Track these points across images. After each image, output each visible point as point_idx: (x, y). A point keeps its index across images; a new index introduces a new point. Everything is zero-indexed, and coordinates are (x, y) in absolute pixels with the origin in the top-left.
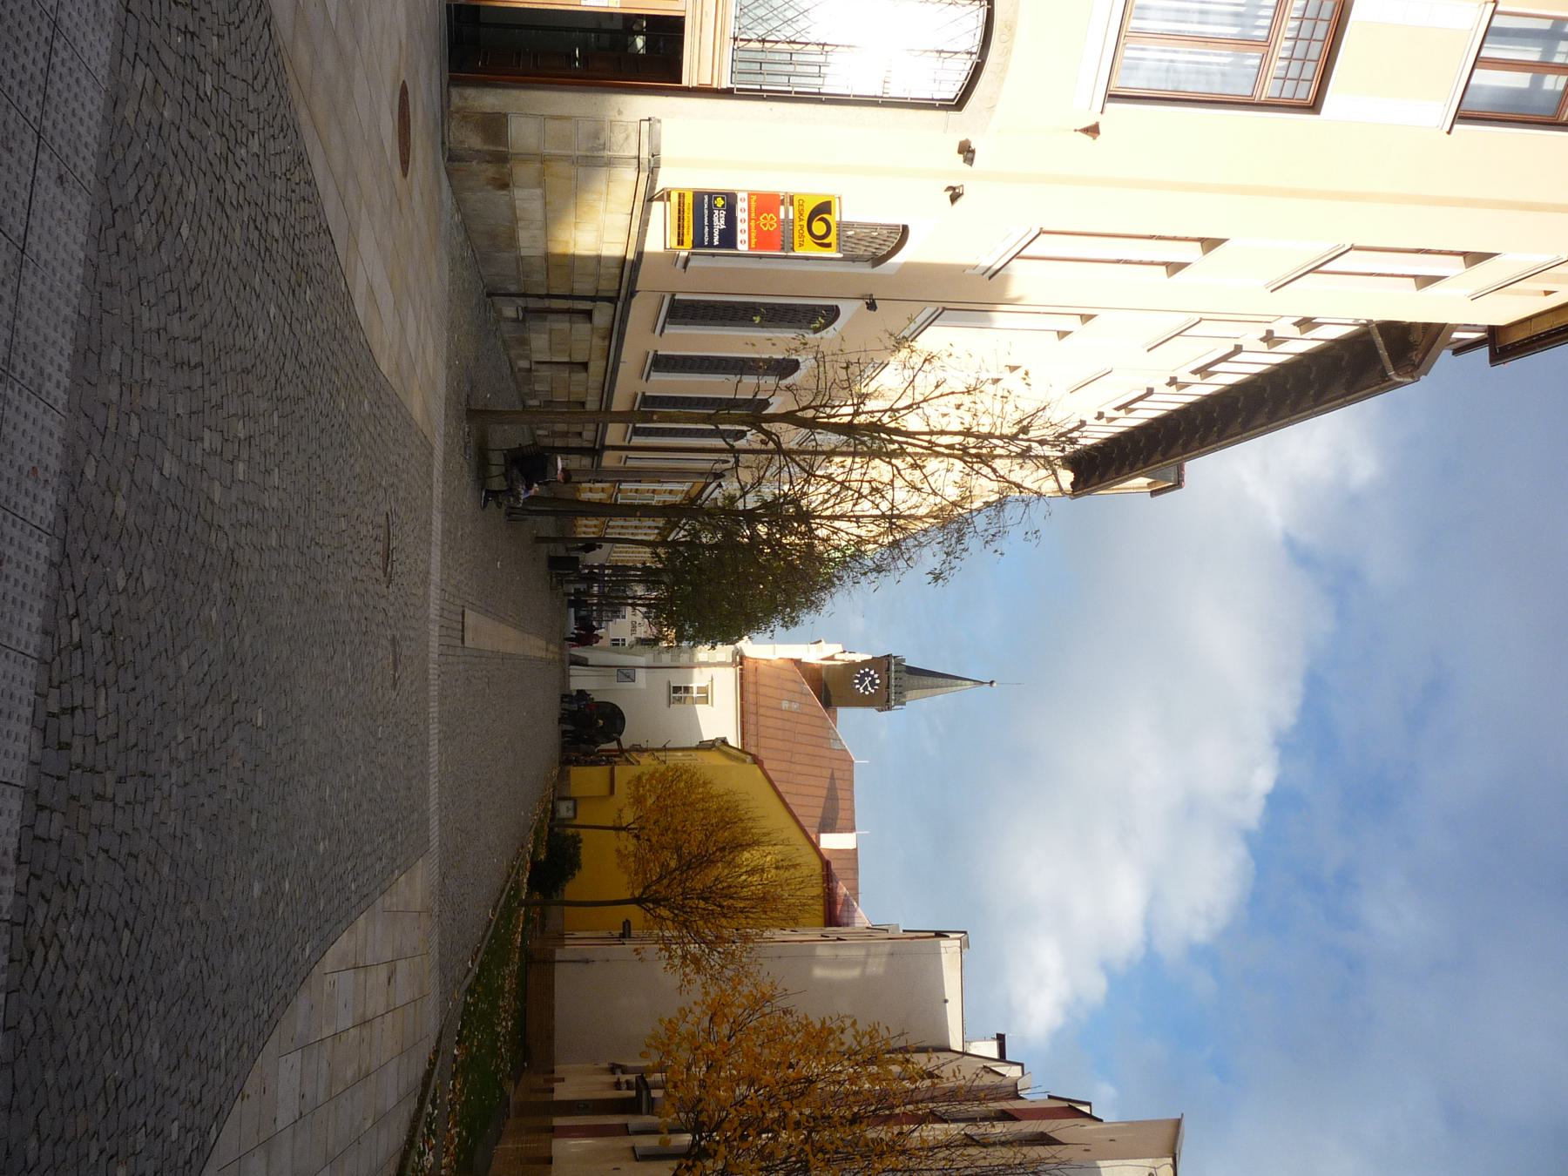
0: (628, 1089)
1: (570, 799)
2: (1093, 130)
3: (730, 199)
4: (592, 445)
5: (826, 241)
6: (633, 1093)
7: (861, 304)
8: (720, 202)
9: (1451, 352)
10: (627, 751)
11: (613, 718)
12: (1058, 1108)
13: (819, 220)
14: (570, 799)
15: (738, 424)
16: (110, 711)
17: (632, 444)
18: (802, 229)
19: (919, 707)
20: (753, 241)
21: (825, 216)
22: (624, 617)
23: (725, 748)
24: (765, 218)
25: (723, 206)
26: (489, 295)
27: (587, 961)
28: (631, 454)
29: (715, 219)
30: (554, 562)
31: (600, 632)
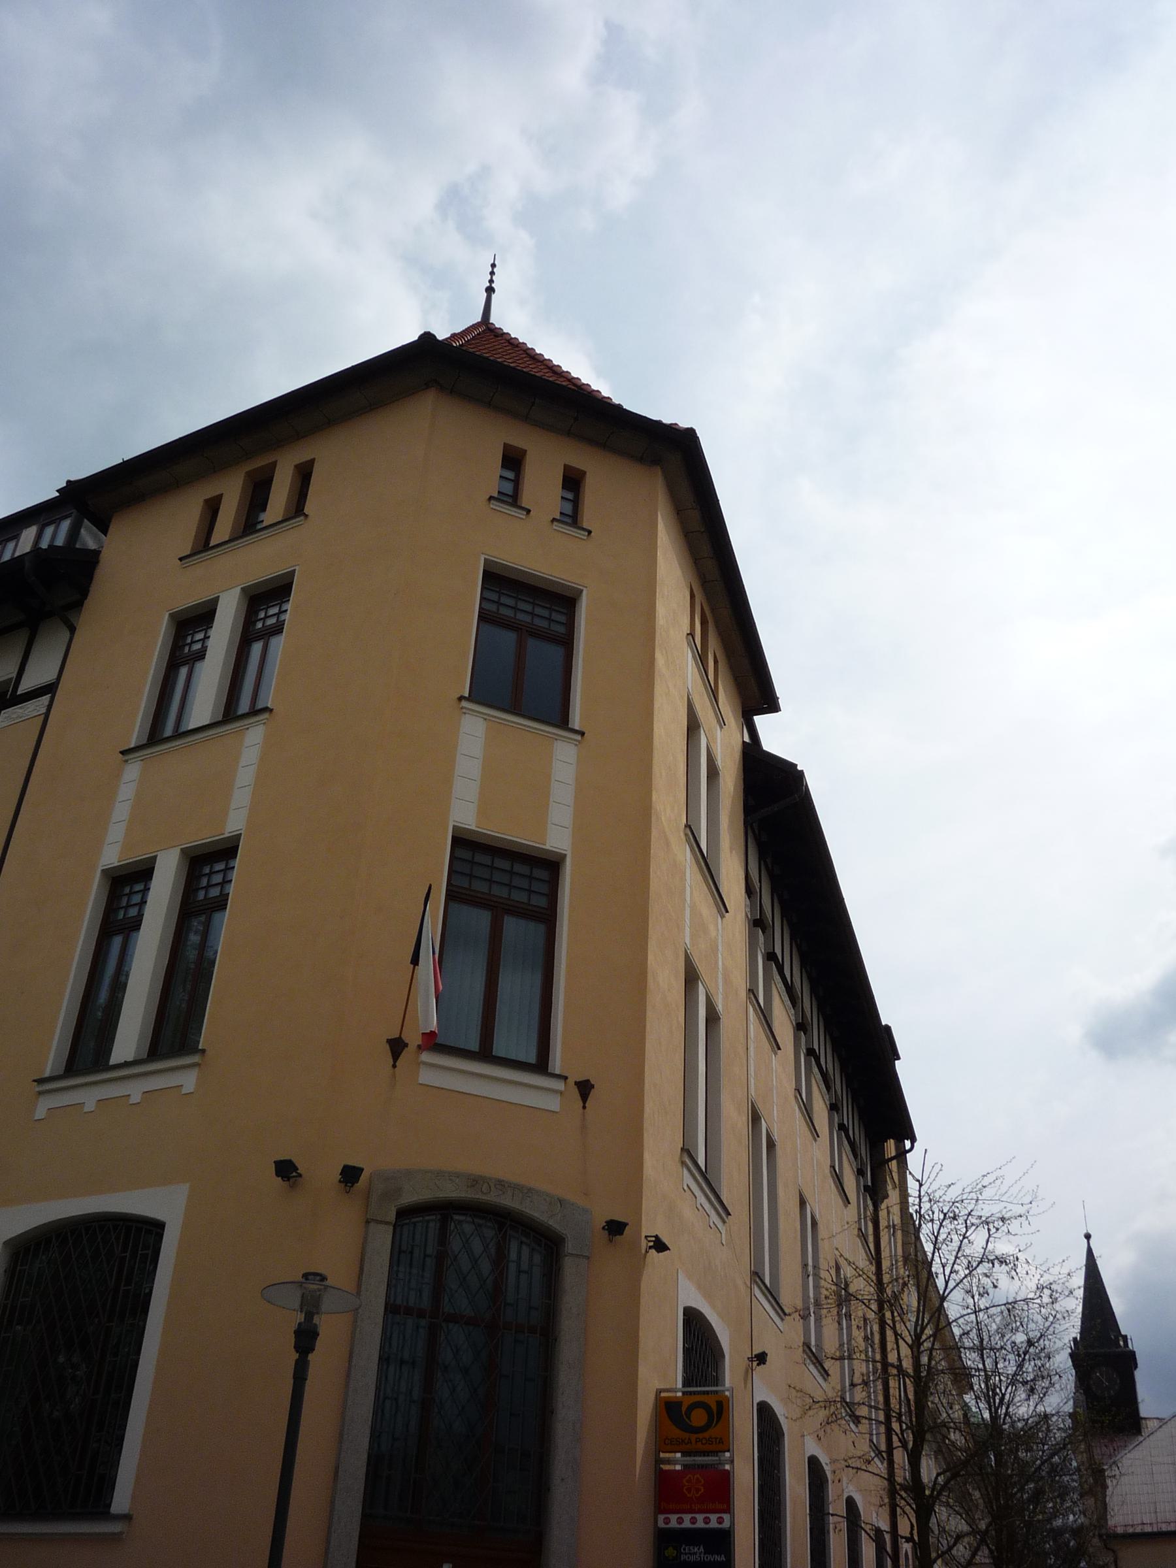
2: (585, 1088)
3: (665, 1538)
7: (760, 1370)
8: (670, 1552)
9: (779, 1051)
13: (689, 1418)
15: (730, 1359)
16: (1064, 1296)
19: (808, 1195)
21: (684, 1409)
24: (689, 1490)
31: (605, 1224)
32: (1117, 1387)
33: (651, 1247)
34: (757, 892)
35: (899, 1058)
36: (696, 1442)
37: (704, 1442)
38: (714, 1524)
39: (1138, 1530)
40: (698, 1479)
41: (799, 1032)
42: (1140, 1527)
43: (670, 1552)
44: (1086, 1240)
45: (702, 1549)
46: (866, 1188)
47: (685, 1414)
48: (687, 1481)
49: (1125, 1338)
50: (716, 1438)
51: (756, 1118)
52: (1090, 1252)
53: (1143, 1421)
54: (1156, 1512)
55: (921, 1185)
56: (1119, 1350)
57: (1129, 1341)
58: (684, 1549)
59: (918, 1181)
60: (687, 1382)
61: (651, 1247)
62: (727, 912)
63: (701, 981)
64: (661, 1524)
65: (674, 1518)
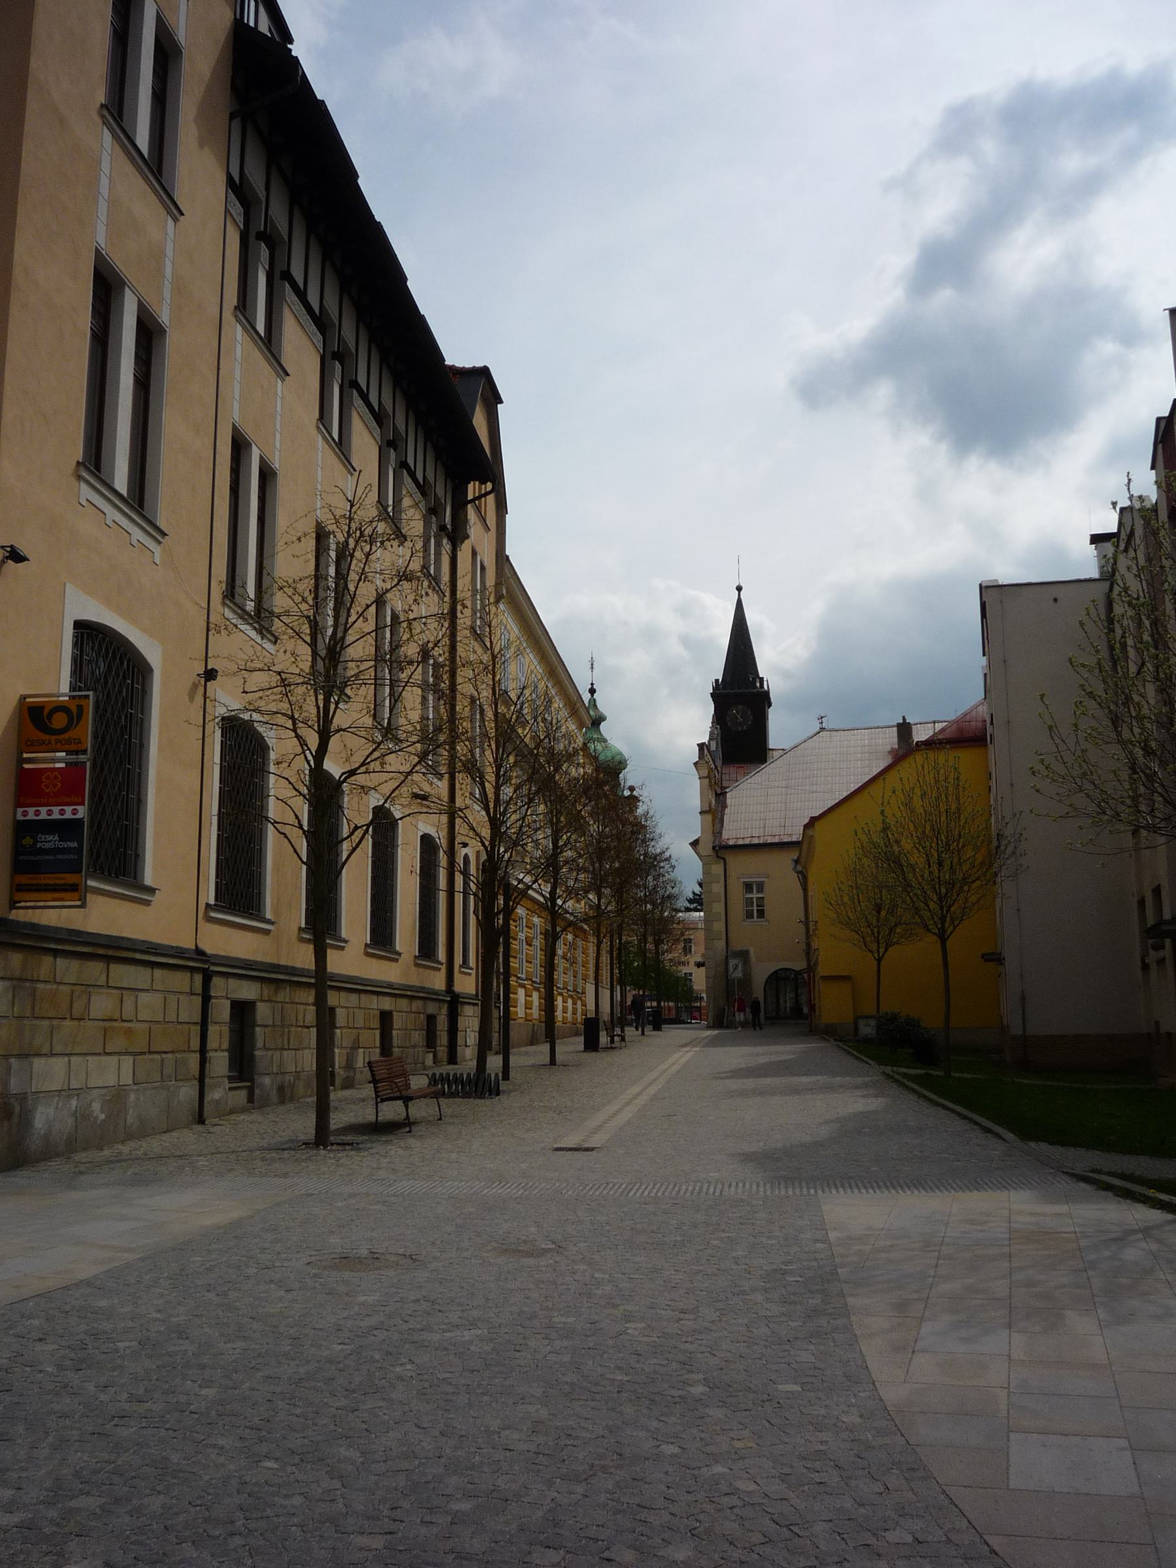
0: (1163, 947)
1: (856, 1024)
3: (22, 829)
4: (446, 1006)
5: (75, 711)
6: (1168, 942)
9: (288, 377)
10: (809, 965)
11: (777, 979)
12: (1163, 452)
14: (856, 1024)
17: (474, 967)
18: (60, 741)
20: (74, 799)
22: (691, 974)
23: (803, 860)
24: (47, 786)
25: (32, 837)
26: (201, 1121)
27: (1023, 999)
28: (458, 959)
29: (47, 846)
30: (592, 1045)
32: (750, 723)
33: (7, 558)
34: (259, 201)
35: (501, 402)
36: (56, 742)
37: (64, 742)
38: (68, 815)
39: (747, 841)
40: (55, 775)
41: (333, 361)
42: (749, 839)
43: (27, 841)
44: (737, 592)
45: (57, 838)
46: (442, 528)
47: (47, 717)
48: (46, 778)
49: (762, 680)
50: (75, 739)
51: (240, 446)
52: (739, 604)
53: (771, 752)
54: (765, 827)
55: (352, 506)
56: (755, 690)
57: (765, 683)
58: (40, 838)
59: (350, 501)
60: (73, 688)
61: (7, 558)
62: (182, 214)
63: (129, 287)
64: (20, 817)
65: (31, 810)
